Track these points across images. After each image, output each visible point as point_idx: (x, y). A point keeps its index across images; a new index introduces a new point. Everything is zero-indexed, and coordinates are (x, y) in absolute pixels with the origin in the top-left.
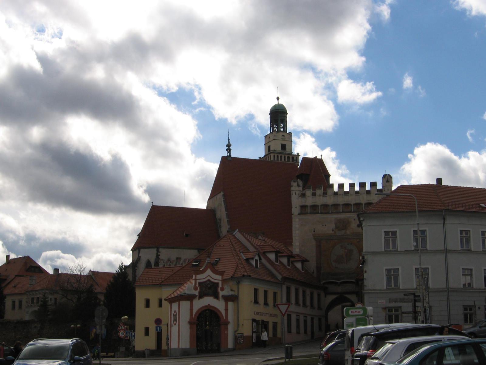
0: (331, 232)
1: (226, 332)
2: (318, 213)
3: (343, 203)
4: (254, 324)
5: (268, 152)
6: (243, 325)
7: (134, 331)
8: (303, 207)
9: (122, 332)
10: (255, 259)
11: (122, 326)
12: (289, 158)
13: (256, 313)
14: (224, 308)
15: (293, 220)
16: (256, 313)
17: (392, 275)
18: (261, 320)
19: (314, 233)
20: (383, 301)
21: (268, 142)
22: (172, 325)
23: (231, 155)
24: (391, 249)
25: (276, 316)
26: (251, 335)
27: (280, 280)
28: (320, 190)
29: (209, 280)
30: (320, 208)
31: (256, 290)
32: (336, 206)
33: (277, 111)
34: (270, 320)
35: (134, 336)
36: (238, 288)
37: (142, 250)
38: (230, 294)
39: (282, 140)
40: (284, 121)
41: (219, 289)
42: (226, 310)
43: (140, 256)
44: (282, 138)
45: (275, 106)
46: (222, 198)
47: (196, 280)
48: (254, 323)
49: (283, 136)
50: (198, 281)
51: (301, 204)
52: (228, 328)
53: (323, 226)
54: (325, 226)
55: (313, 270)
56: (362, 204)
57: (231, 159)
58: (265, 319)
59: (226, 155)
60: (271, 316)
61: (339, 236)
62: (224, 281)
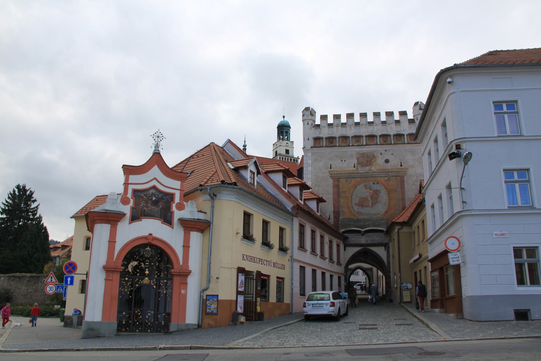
1: (183, 292)
2: (336, 146)
3: (367, 134)
4: (242, 278)
6: (217, 278)
9: (51, 286)
10: (249, 171)
11: (52, 277)
12: (291, 159)
13: (245, 257)
14: (182, 244)
16: (245, 257)
17: (516, 182)
18: (255, 271)
19: (330, 170)
21: (276, 148)
26: (235, 299)
30: (339, 141)
31: (247, 216)
32: (357, 138)
34: (273, 273)
36: (213, 207)
38: (196, 218)
39: (286, 146)
40: (288, 133)
41: (174, 205)
42: (186, 247)
44: (286, 145)
45: (281, 122)
48: (240, 274)
49: (287, 143)
50: (131, 188)
51: (315, 136)
54: (345, 161)
55: (329, 216)
56: (390, 136)
58: (265, 270)
60: (274, 266)
61: (363, 173)
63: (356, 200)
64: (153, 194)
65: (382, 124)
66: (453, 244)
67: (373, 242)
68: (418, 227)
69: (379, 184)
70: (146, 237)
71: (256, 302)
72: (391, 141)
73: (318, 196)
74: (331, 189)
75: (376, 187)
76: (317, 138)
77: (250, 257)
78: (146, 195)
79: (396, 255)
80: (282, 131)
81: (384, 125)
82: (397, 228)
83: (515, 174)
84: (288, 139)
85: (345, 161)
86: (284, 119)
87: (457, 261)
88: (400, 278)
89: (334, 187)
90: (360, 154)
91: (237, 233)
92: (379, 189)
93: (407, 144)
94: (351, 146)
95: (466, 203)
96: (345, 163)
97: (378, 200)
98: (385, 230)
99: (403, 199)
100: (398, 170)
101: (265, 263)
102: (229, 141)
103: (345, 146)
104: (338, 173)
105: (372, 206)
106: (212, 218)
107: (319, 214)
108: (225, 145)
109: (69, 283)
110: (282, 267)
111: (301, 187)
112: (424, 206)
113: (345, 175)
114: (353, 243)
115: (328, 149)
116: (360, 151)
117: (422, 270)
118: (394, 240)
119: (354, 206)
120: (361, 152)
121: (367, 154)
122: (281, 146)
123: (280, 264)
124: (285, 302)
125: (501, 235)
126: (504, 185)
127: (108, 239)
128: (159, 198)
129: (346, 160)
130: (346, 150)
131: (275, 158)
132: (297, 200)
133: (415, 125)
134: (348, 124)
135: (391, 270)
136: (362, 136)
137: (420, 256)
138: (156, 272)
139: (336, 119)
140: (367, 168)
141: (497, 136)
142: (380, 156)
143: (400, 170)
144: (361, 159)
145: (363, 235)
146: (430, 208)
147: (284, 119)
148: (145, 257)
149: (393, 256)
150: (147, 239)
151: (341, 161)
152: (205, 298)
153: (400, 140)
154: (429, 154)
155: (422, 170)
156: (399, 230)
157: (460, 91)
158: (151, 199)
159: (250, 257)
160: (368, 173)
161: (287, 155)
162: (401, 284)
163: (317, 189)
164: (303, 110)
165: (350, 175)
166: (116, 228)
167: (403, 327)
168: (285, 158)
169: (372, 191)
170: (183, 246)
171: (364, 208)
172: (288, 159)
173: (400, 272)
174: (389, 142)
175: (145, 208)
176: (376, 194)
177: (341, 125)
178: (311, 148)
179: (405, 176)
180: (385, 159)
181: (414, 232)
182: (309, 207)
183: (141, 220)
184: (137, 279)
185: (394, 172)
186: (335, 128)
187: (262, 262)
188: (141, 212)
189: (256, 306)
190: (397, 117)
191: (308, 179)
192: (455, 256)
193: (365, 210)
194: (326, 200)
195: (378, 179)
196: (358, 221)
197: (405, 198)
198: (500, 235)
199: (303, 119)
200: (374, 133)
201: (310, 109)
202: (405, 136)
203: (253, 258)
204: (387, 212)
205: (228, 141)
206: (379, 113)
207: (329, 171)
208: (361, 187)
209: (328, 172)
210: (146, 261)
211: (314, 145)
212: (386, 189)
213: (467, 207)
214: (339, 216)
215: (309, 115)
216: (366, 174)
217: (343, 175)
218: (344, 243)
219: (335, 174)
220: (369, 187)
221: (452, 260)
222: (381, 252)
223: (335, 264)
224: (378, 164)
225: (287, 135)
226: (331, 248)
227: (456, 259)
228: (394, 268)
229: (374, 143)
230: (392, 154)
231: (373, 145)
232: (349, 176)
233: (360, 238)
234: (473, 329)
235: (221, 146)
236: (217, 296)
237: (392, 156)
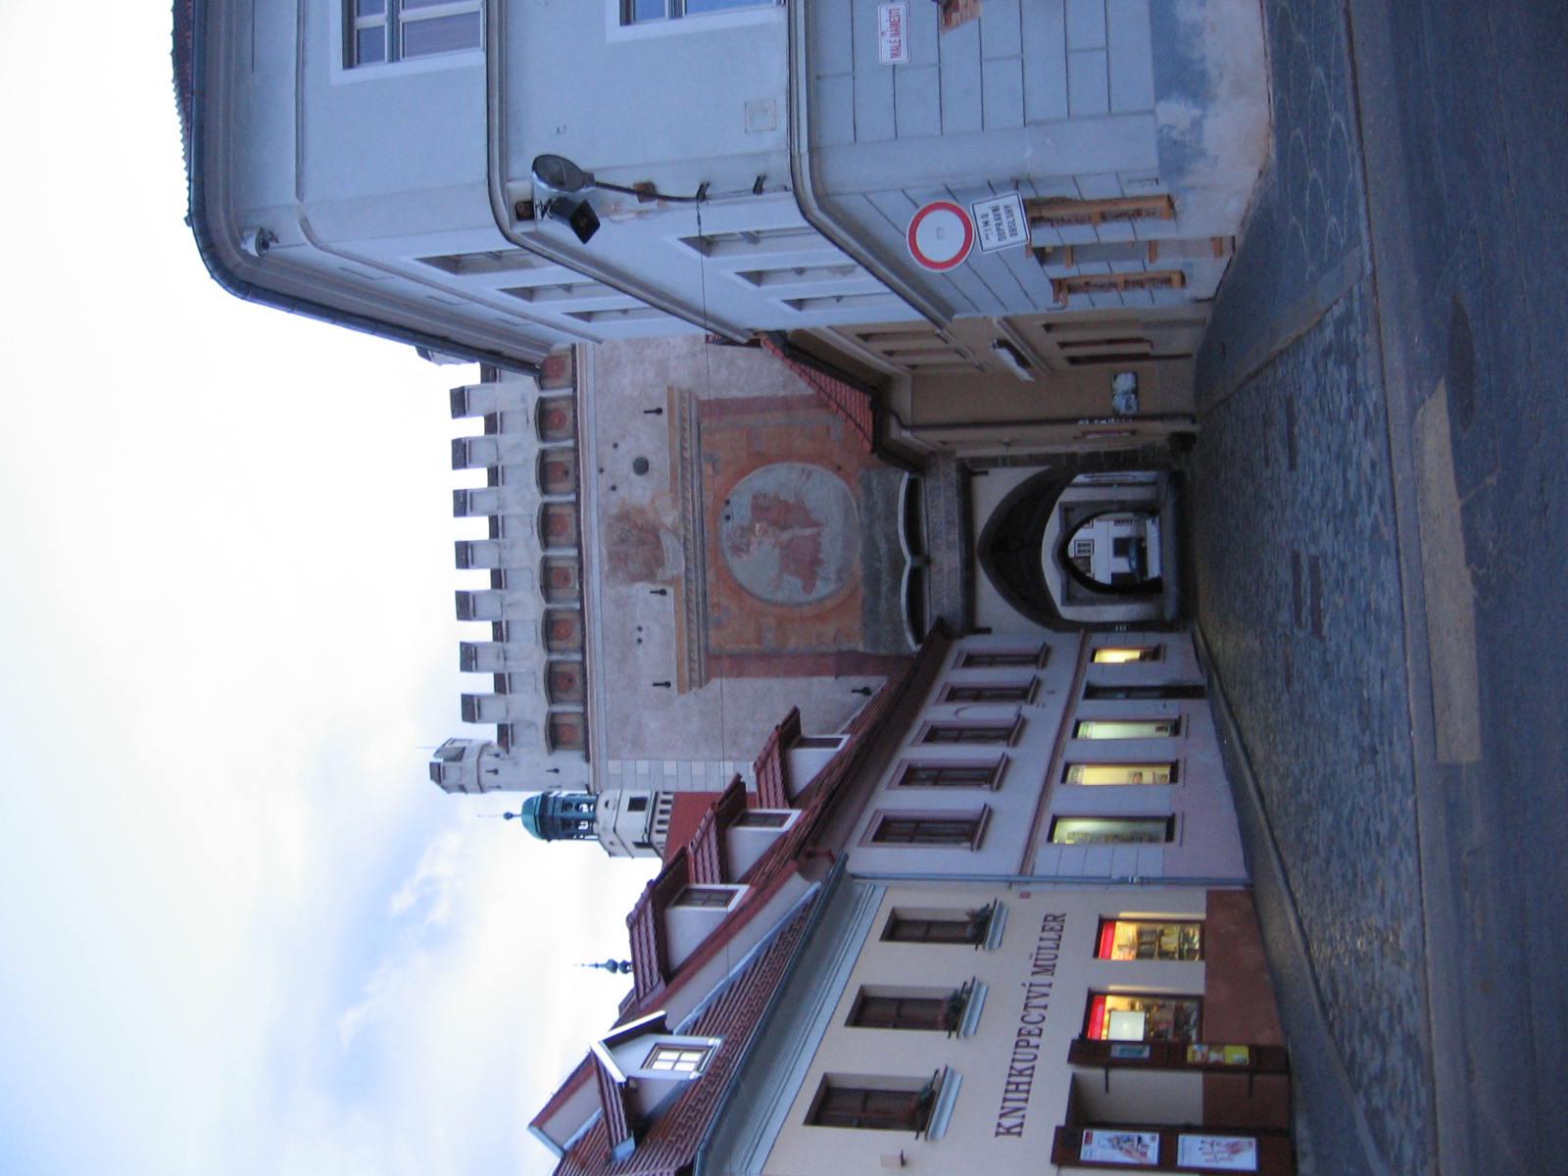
3: (536, 541)
8: (556, 736)
13: (1007, 1122)
15: (697, 788)
16: (1007, 1122)
19: (674, 685)
20: (885, 24)
25: (1054, 923)
27: (817, 885)
28: (479, 655)
32: (550, 579)
33: (538, 819)
44: (614, 809)
45: (526, 825)
48: (1087, 1153)
49: (606, 804)
54: (640, 629)
55: (854, 691)
56: (543, 454)
60: (1049, 969)
63: (791, 589)
65: (500, 483)
66: (939, 233)
67: (957, 523)
68: (890, 353)
69: (728, 497)
71: (1204, 1067)
72: (563, 450)
73: (774, 743)
74: (750, 687)
76: (551, 735)
77: (1009, 1096)
79: (1007, 433)
80: (559, 822)
81: (503, 474)
82: (899, 434)
86: (516, 816)
87: (1009, 211)
88: (1096, 422)
89: (740, 674)
90: (614, 569)
91: (903, 1163)
92: (751, 499)
93: (575, 390)
95: (765, 177)
97: (792, 500)
98: (906, 476)
99: (788, 404)
101: (1034, 1015)
102: (540, 1123)
103: (583, 629)
104: (686, 657)
105: (816, 525)
107: (846, 738)
108: (555, 1143)
110: (1052, 929)
111: (732, 818)
112: (801, 334)
113: (695, 628)
115: (591, 696)
117: (1060, 340)
118: (944, 443)
119: (814, 595)
120: (606, 568)
121: (615, 544)
123: (1041, 939)
124: (1198, 987)
125: (897, 33)
126: (688, 24)
130: (598, 625)
131: (662, 852)
132: (784, 837)
134: (499, 613)
135: (1062, 449)
136: (545, 561)
137: (1003, 343)
139: (479, 661)
140: (669, 542)
142: (622, 492)
143: (677, 413)
144: (631, 567)
145: (928, 561)
146: (803, 313)
147: (516, 816)
149: (1008, 444)
151: (641, 646)
153: (562, 418)
154: (587, 316)
156: (903, 426)
159: (1009, 1096)
160: (685, 539)
161: (650, 805)
162: (1117, 415)
163: (749, 740)
164: (443, 787)
165: (694, 608)
167: (1302, 441)
169: (758, 526)
171: (822, 556)
173: (1075, 420)
174: (570, 456)
176: (767, 509)
178: (587, 760)
179: (697, 397)
180: (633, 476)
181: (913, 367)
182: (818, 780)
185: (683, 439)
186: (513, 667)
187: (1029, 1033)
189: (1220, 1068)
190: (473, 427)
191: (713, 777)
193: (832, 551)
194: (791, 708)
195: (708, 501)
196: (872, 579)
197: (785, 398)
198: (895, 35)
199: (474, 791)
200: (531, 516)
201: (439, 765)
202: (546, 394)
203: (1013, 1079)
204: (839, 468)
205: (535, 1129)
206: (456, 493)
208: (742, 568)
209: (683, 697)
211: (580, 749)
213: (779, 166)
214: (852, 653)
215: (461, 768)
216: (690, 547)
218: (961, 636)
219: (691, 670)
220: (742, 536)
222: (994, 491)
223: (1042, 674)
224: (653, 501)
226: (978, 695)
228: (1058, 442)
229: (570, 515)
230: (616, 446)
231: (578, 519)
232: (699, 612)
233: (941, 570)
234: (1305, 151)
235: (558, 1160)
237: (623, 447)
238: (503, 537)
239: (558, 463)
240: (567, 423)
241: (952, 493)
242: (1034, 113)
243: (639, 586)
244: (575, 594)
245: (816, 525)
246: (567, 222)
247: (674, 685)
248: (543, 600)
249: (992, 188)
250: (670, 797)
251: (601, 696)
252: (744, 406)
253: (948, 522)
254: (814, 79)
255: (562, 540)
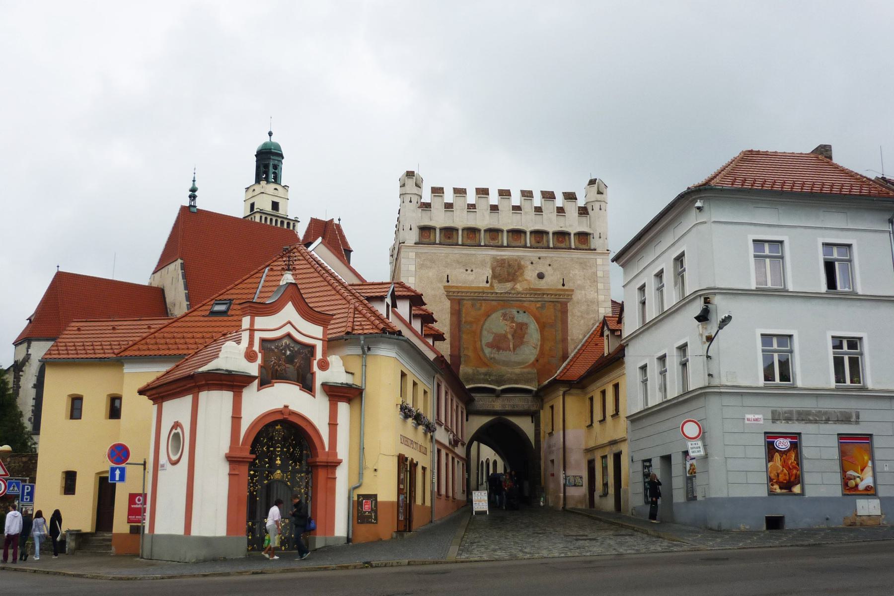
0: (485, 285)
5: (251, 212)
7: (33, 480)
12: (282, 223)
14: (327, 420)
20: (757, 416)
21: (252, 197)
22: (163, 466)
23: (196, 205)
24: (769, 285)
29: (289, 335)
32: (494, 232)
33: (268, 150)
35: (31, 494)
37: (34, 344)
41: (315, 363)
42: (333, 425)
43: (29, 353)
45: (265, 144)
46: (180, 269)
47: (252, 330)
49: (276, 189)
50: (258, 336)
52: (335, 478)
53: (467, 270)
54: (472, 271)
56: (547, 233)
57: (196, 211)
59: (188, 205)
61: (501, 293)
62: (331, 344)
63: (487, 338)
64: (287, 347)
65: (536, 213)
69: (527, 313)
70: (281, 411)
72: (548, 242)
75: (521, 318)
78: (277, 347)
83: (775, 341)
84: (277, 180)
85: (472, 271)
87: (698, 452)
90: (497, 261)
93: (574, 249)
94: (482, 246)
96: (472, 274)
97: (525, 340)
99: (564, 340)
100: (558, 293)
105: (514, 349)
106: (364, 382)
109: (117, 478)
113: (472, 295)
114: (481, 409)
116: (498, 255)
119: (484, 347)
120: (498, 258)
121: (508, 262)
122: (263, 193)
127: (231, 414)
128: (296, 352)
129: (474, 269)
133: (588, 219)
136: (502, 231)
138: (291, 462)
140: (509, 285)
141: (756, 288)
142: (530, 267)
145: (498, 396)
148: (275, 440)
150: (283, 414)
151: (465, 271)
152: (356, 498)
153: (562, 242)
155: (596, 294)
157: (712, 221)
158: (285, 354)
160: (510, 293)
161: (274, 213)
165: (480, 295)
166: (241, 396)
168: (271, 220)
169: (514, 325)
170: (329, 424)
172: (276, 221)
175: (277, 367)
176: (521, 329)
177: (468, 209)
178: (415, 244)
180: (537, 272)
183: (273, 386)
184: (267, 472)
185: (552, 295)
188: (272, 373)
192: (696, 446)
195: (526, 304)
197: (567, 339)
207: (445, 287)
208: (496, 317)
210: (277, 445)
212: (538, 323)
213: (715, 382)
217: (467, 295)
219: (454, 292)
221: (692, 450)
222: (526, 425)
224: (526, 280)
225: (276, 171)
227: (696, 450)
230: (550, 265)
232: (478, 297)
233: (494, 402)
236: (376, 496)
237: (550, 268)
238: (512, 213)
239: (543, 238)
240: (559, 244)
241: (526, 407)
242: (729, 461)
243: (491, 272)
244: (487, 243)
245: (514, 349)
246: (701, 314)
247: (447, 284)
248: (485, 228)
249: (705, 446)
250: (291, 228)
251: (443, 252)
252: (565, 322)
253: (514, 405)
254: (742, 394)
255: (510, 239)
